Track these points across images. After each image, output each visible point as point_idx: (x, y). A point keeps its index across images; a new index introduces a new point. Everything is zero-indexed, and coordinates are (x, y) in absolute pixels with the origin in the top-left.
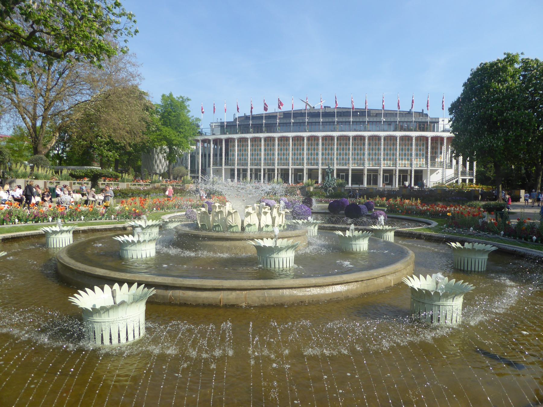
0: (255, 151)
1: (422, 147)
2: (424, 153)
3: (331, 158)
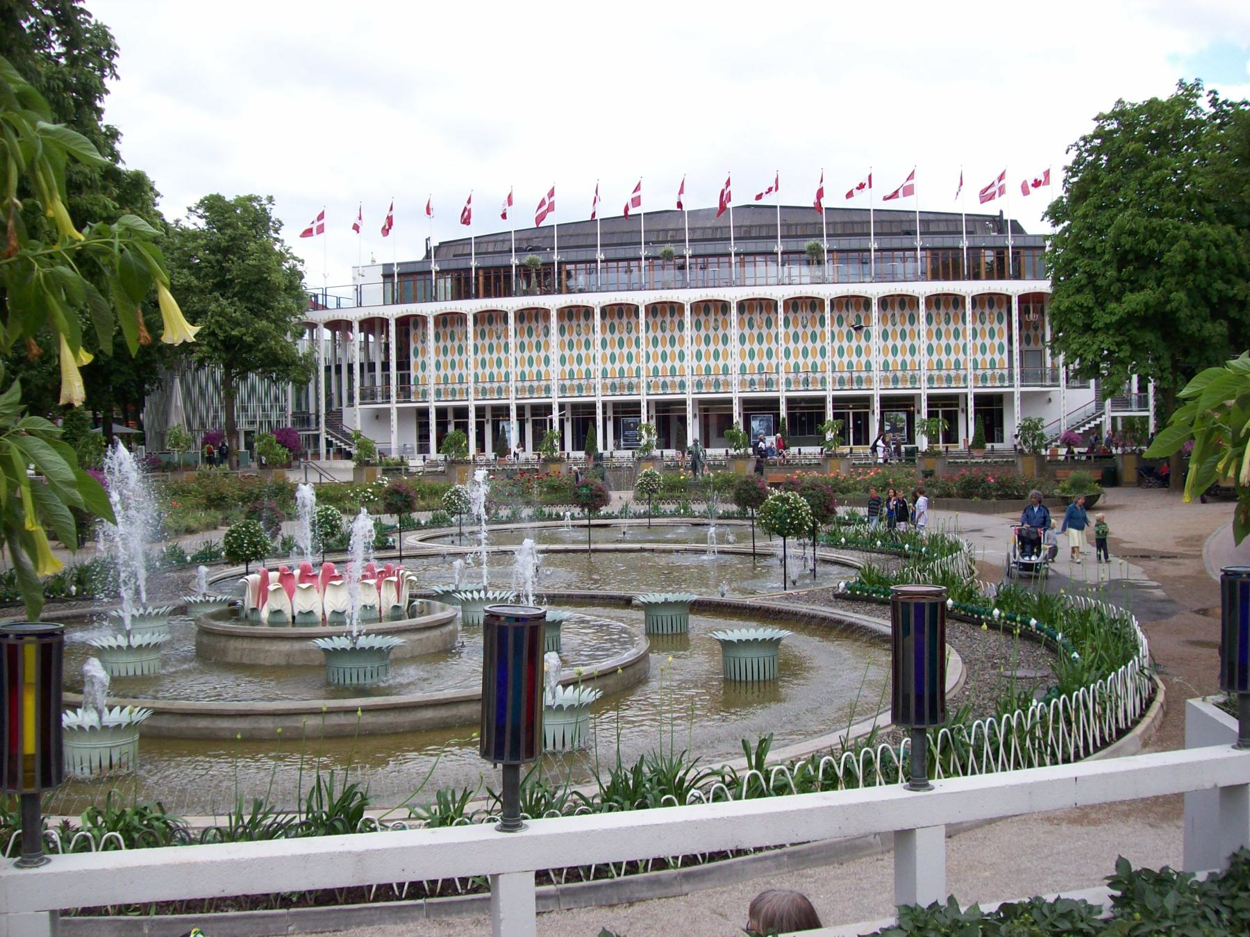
1: (996, 326)
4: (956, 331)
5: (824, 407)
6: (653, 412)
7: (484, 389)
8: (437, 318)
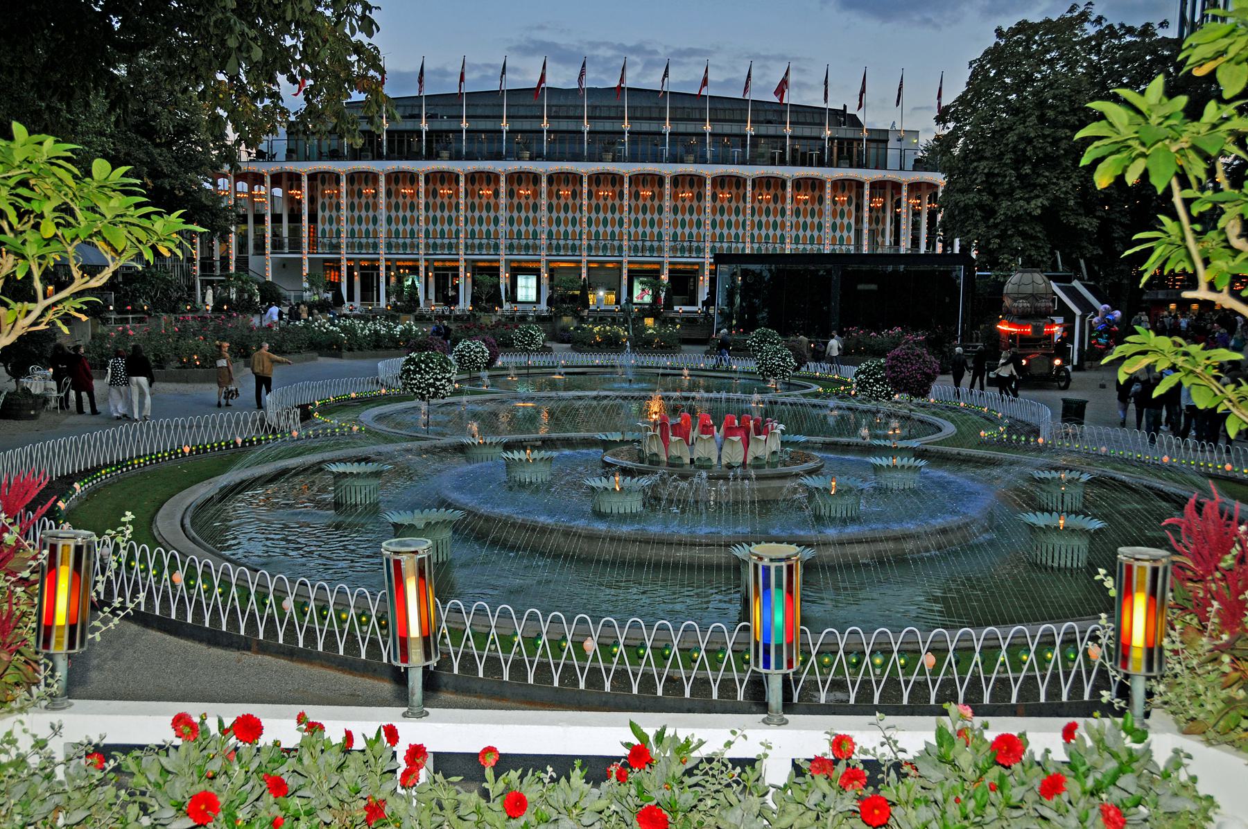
0: (768, 216)
2: (853, 221)
3: (412, 231)
4: (737, 209)
7: (435, 244)
8: (714, 180)
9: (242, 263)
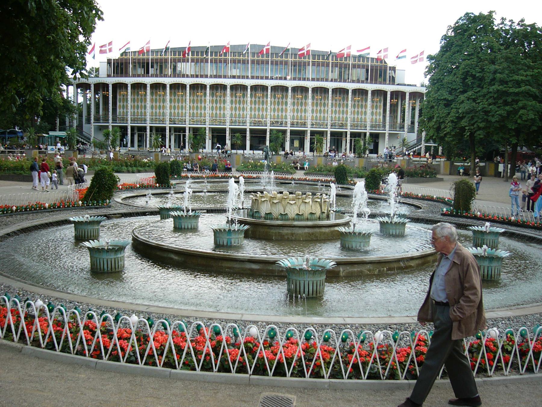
5: (266, 134)
6: (191, 132)
9: (80, 127)
